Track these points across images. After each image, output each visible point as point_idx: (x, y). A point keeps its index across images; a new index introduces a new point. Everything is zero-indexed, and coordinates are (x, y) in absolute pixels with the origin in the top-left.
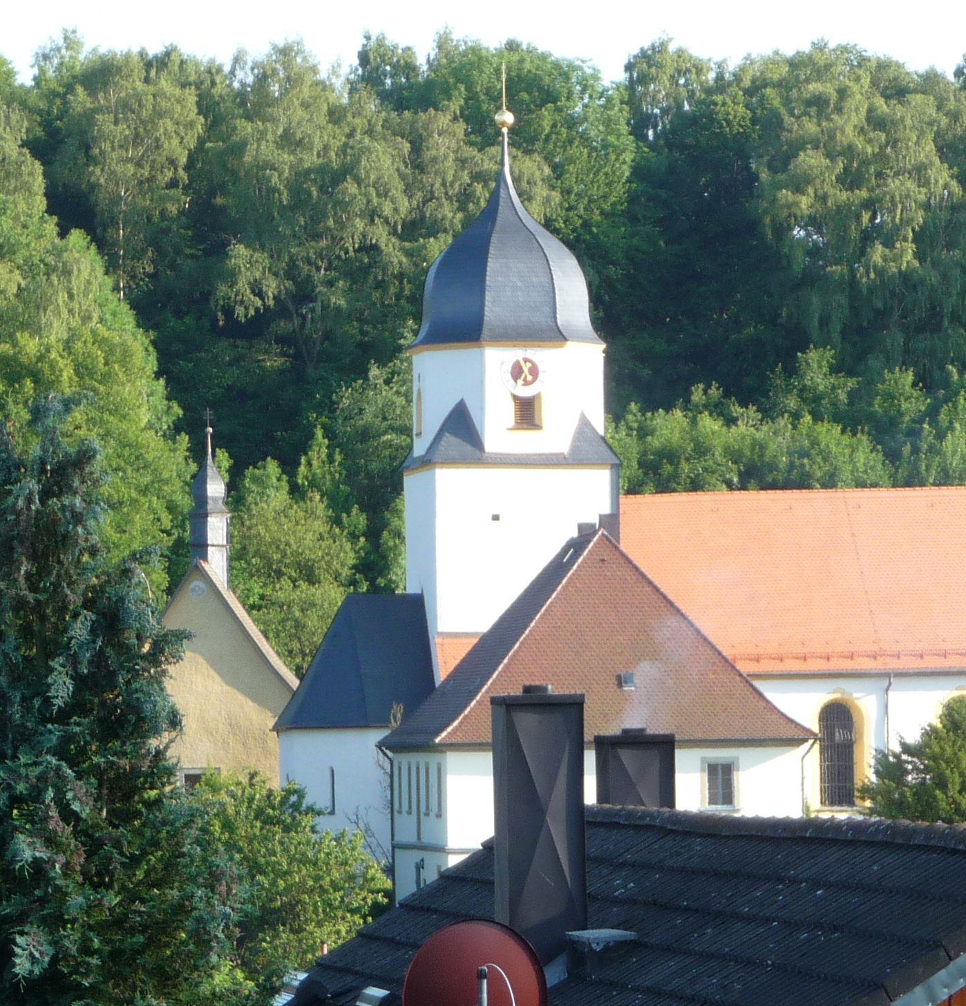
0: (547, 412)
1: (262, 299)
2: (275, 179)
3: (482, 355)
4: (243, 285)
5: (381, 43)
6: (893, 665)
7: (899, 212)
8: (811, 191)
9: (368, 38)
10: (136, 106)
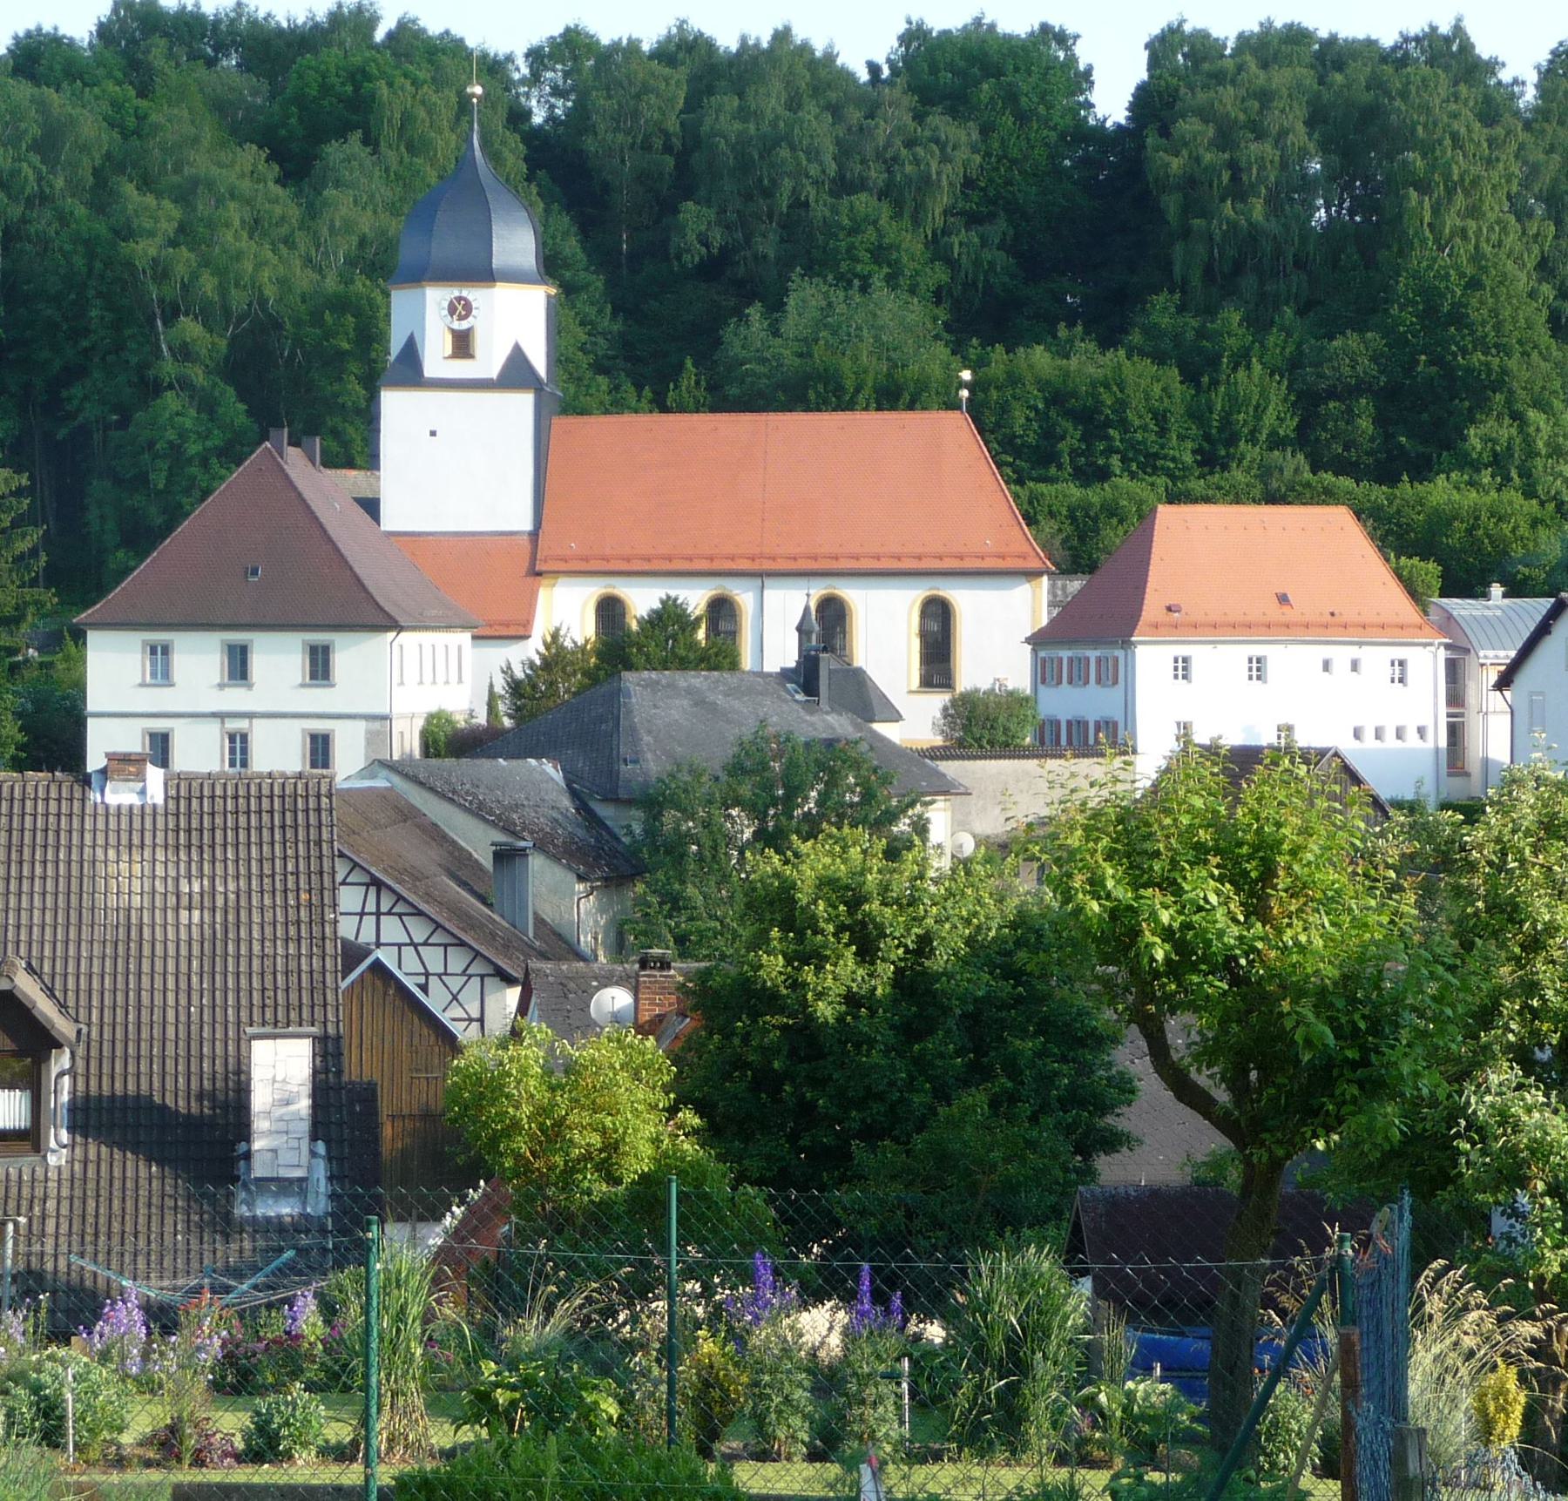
0: (479, 344)
1: (708, 248)
2: (722, 145)
3: (424, 294)
4: (691, 237)
5: (920, 26)
6: (767, 565)
7: (1254, 171)
8: (1185, 153)
9: (910, 22)
10: (626, 84)
